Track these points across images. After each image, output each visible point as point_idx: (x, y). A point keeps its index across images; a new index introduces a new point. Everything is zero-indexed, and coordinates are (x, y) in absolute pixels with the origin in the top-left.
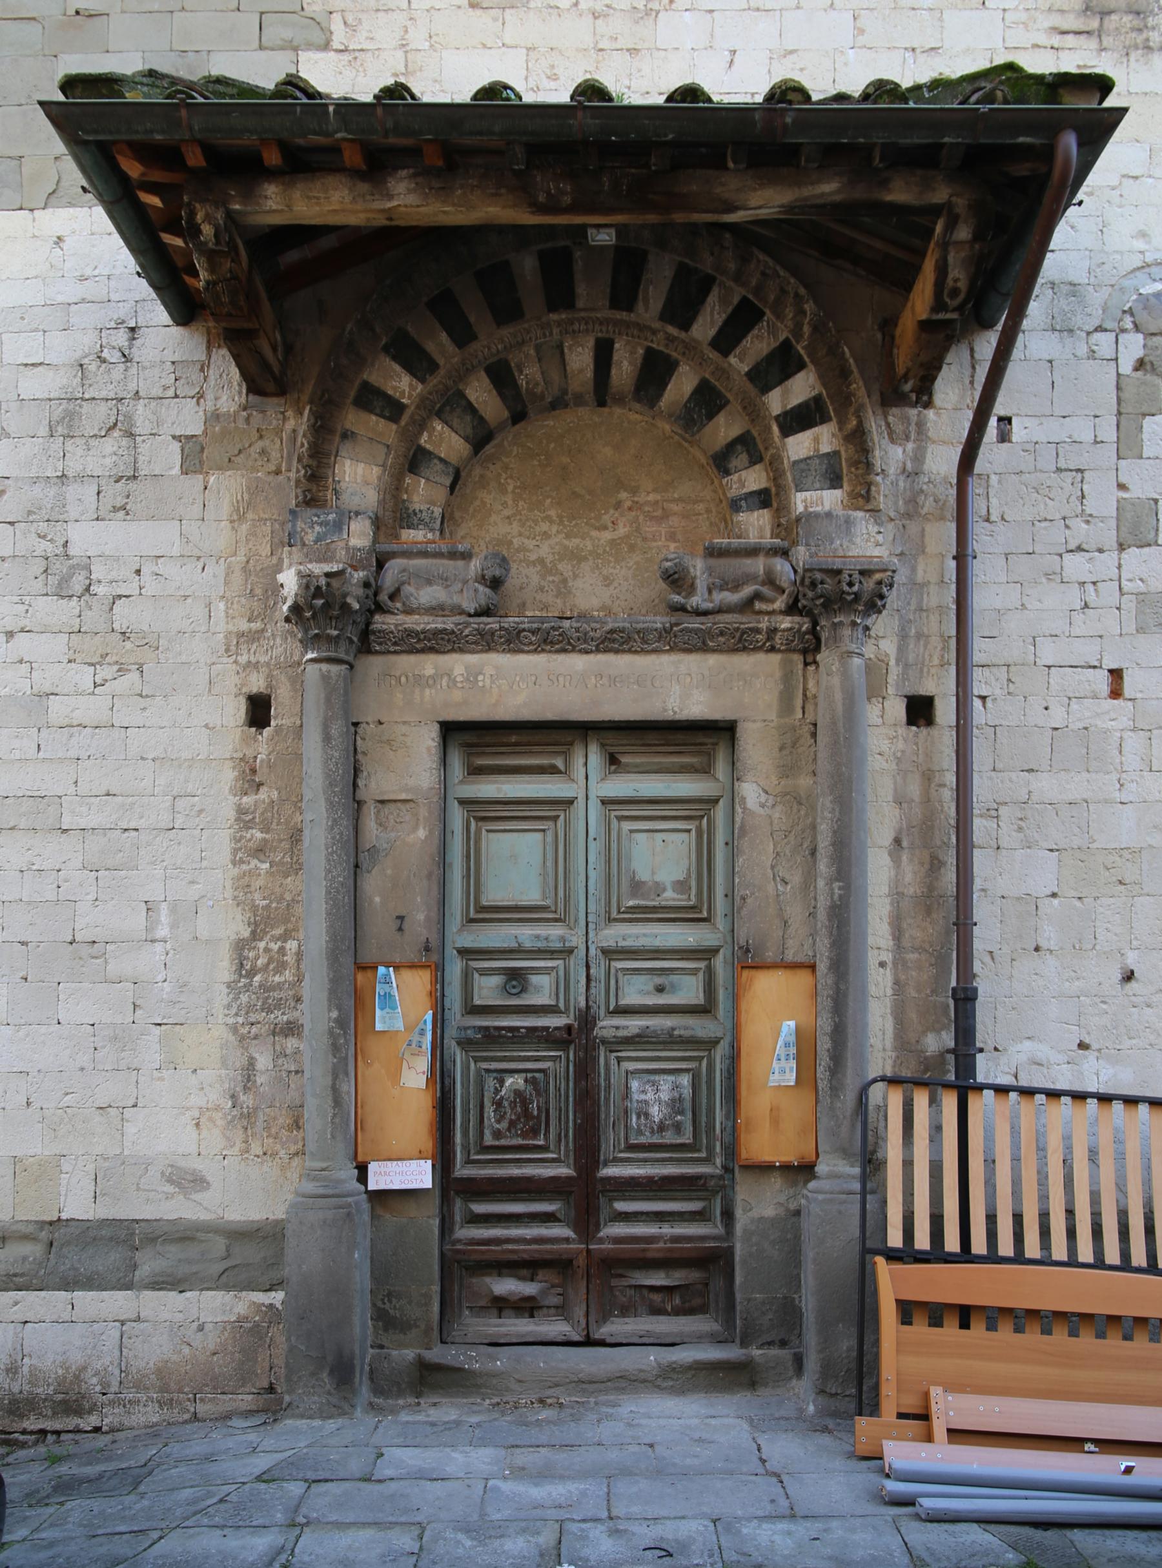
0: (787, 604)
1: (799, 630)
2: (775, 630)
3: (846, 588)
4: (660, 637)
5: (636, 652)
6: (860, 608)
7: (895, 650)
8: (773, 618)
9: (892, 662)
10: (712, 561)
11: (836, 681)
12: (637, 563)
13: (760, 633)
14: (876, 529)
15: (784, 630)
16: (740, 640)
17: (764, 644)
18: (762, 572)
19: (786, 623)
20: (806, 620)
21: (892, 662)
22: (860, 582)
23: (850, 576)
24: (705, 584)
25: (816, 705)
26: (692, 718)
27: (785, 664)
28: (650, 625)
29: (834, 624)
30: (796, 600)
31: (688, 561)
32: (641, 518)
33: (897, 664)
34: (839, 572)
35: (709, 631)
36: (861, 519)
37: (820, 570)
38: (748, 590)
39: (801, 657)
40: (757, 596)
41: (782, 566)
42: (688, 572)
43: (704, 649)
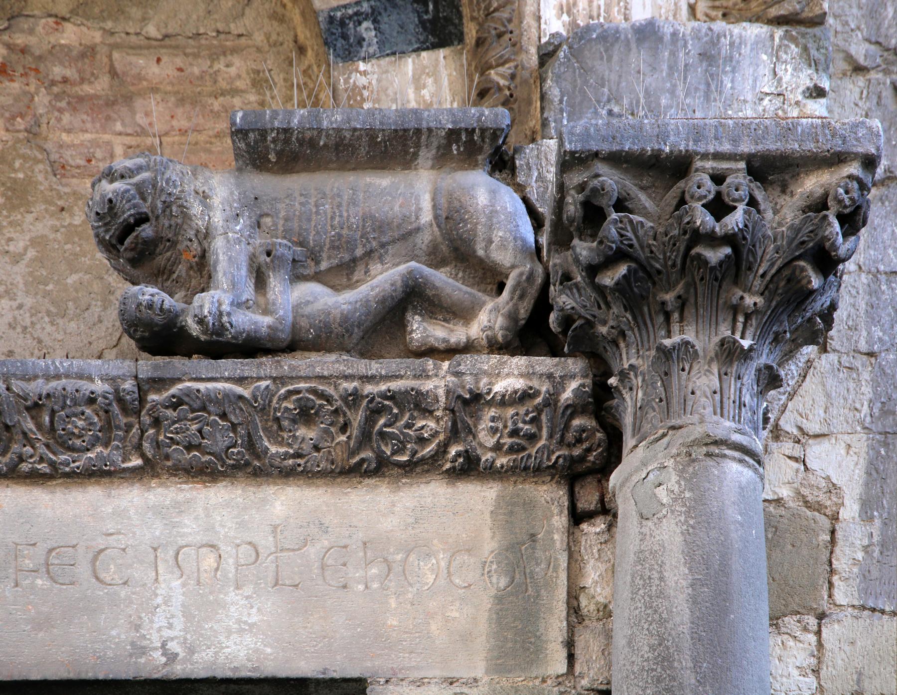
0: (512, 317)
1: (551, 401)
2: (473, 401)
3: (703, 219)
4: (108, 426)
5: (34, 478)
6: (750, 300)
7: (859, 474)
8: (467, 362)
9: (850, 511)
10: (265, 184)
11: (669, 533)
12: (38, 242)
13: (428, 412)
14: (806, 78)
15: (504, 401)
16: (366, 437)
17: (443, 449)
18: (426, 217)
19: (510, 375)
20: (575, 365)
21: (850, 511)
22: (752, 202)
23: (718, 179)
24: (242, 254)
25: (608, 635)
26: (223, 672)
27: (506, 513)
28: (70, 385)
29: (665, 354)
30: (543, 305)
31: (181, 178)
32: (42, 100)
33: (866, 516)
34: (677, 167)
35: (262, 406)
36: (758, 43)
37: (616, 159)
38: (382, 279)
39: (561, 494)
40: (414, 297)
41: (493, 193)
42: (186, 217)
43: (248, 465)
